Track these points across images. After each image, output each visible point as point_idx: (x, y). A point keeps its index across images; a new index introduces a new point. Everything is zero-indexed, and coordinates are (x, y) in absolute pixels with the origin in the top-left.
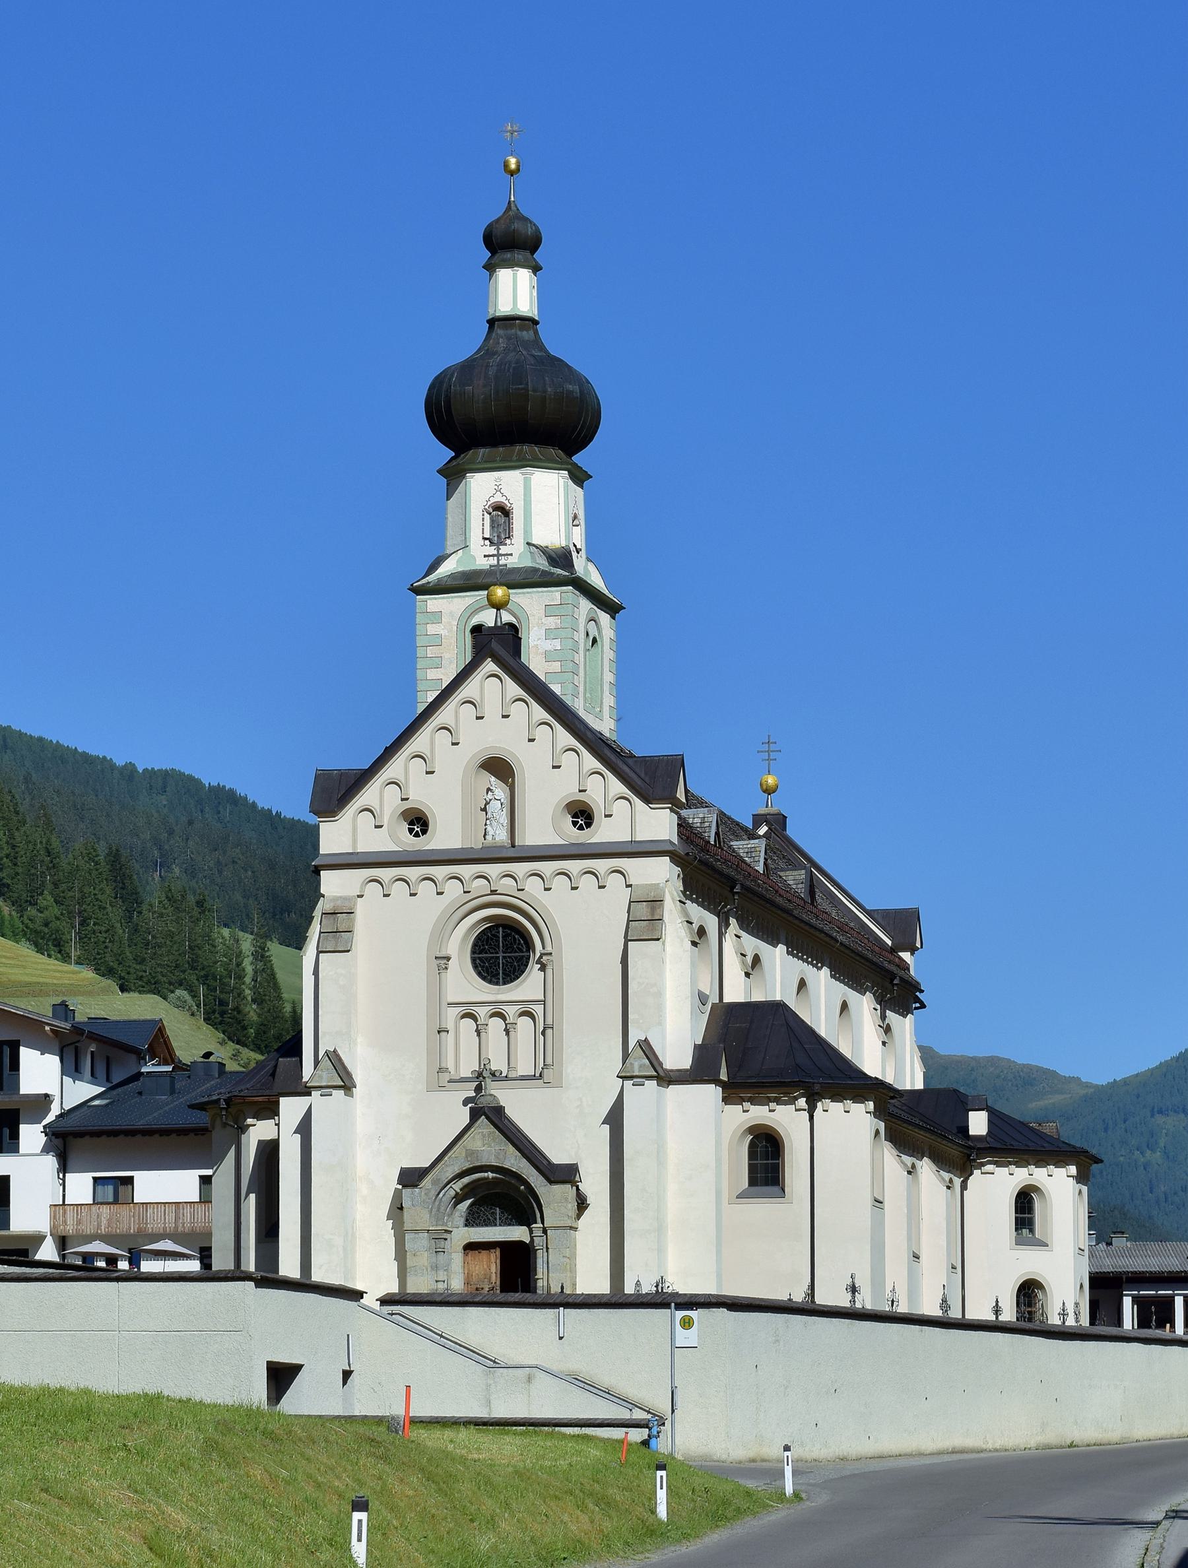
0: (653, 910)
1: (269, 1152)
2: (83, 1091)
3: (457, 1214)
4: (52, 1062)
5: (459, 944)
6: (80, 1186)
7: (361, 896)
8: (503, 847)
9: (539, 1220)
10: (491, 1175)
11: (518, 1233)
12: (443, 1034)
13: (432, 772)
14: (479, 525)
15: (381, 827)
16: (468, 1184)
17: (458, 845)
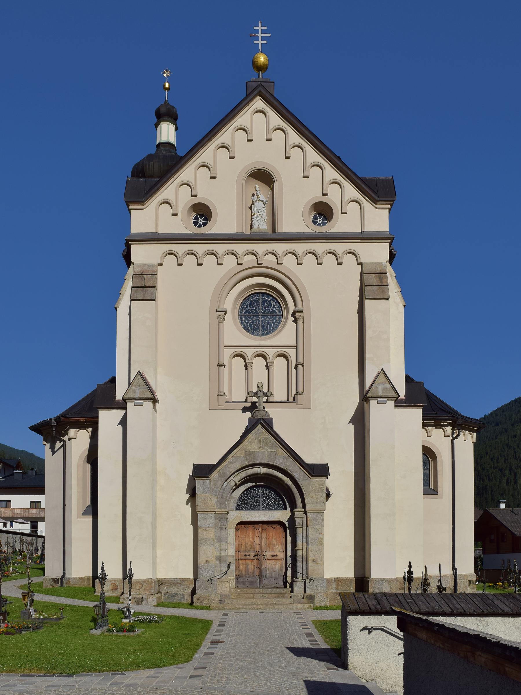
0: (381, 279)
3: (232, 500)
5: (231, 303)
7: (161, 265)
12: (221, 368)
13: (215, 178)
15: (176, 215)
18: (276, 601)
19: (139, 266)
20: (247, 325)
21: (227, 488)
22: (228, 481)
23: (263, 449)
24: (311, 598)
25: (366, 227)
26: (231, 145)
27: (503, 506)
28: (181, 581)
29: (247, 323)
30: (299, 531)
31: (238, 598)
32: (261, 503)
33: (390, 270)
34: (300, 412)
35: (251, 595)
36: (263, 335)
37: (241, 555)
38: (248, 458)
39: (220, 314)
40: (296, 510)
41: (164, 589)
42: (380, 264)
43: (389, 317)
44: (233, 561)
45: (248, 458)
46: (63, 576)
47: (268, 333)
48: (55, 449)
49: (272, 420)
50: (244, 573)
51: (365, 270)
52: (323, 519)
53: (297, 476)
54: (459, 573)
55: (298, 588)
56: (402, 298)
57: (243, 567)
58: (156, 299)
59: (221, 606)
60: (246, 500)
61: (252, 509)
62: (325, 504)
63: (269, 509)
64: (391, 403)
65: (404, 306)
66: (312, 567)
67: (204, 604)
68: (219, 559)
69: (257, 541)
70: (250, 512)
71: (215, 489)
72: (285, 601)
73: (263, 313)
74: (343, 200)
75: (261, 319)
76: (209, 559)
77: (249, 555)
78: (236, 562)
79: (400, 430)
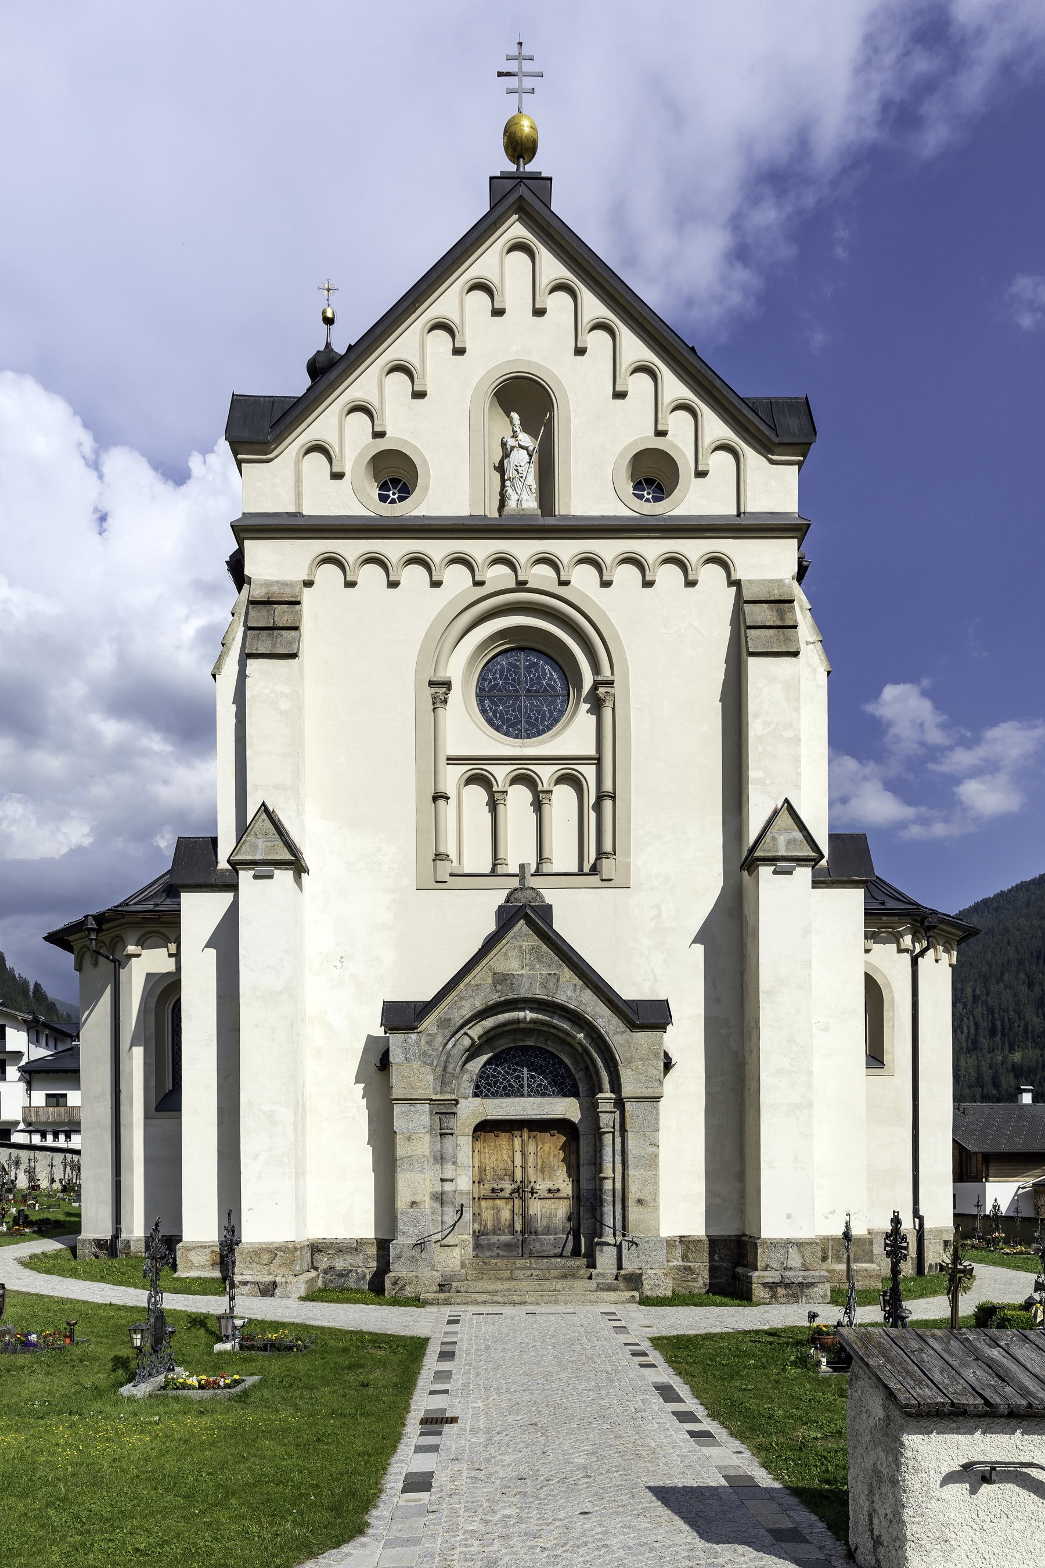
0: (781, 615)
1: (166, 993)
2: (40, 1052)
3: (466, 1077)
4: (23, 1036)
5: (460, 666)
6: (39, 1098)
7: (308, 584)
8: (532, 516)
9: (606, 1085)
10: (529, 1015)
12: (441, 803)
16: (493, 1029)
17: (465, 512)
18: (559, 1285)
19: (262, 585)
20: (495, 717)
21: (454, 1051)
22: (457, 1036)
23: (532, 968)
24: (634, 1281)
25: (749, 502)
26: (457, 321)
27: (1027, 1098)
28: (357, 1247)
29: (495, 711)
30: (607, 1139)
31: (478, 1278)
32: (526, 1083)
33: (798, 592)
34: (607, 894)
35: (507, 1273)
36: (528, 737)
37: (485, 1189)
38: (499, 987)
39: (437, 690)
40: (600, 1095)
41: (324, 1262)
42: (780, 582)
43: (792, 697)
44: (466, 1200)
45: (499, 987)
46: (116, 1236)
47: (539, 733)
49: (550, 907)
50: (490, 1225)
51: (747, 595)
52: (658, 1114)
53: (602, 1024)
54: (927, 1225)
55: (606, 1259)
56: (823, 657)
57: (488, 1215)
58: (300, 654)
59: (442, 1296)
60: (494, 1076)
61: (508, 1095)
62: (661, 1083)
63: (543, 1095)
64: (804, 874)
65: (829, 673)
66: (634, 1213)
67: (409, 1292)
68: (440, 1198)
69: (518, 1161)
70: (502, 1100)
71: (430, 1052)
72: (578, 1284)
73: (528, 691)
74: (700, 444)
75: (524, 702)
76: (418, 1199)
77: (502, 1190)
78: (474, 1203)
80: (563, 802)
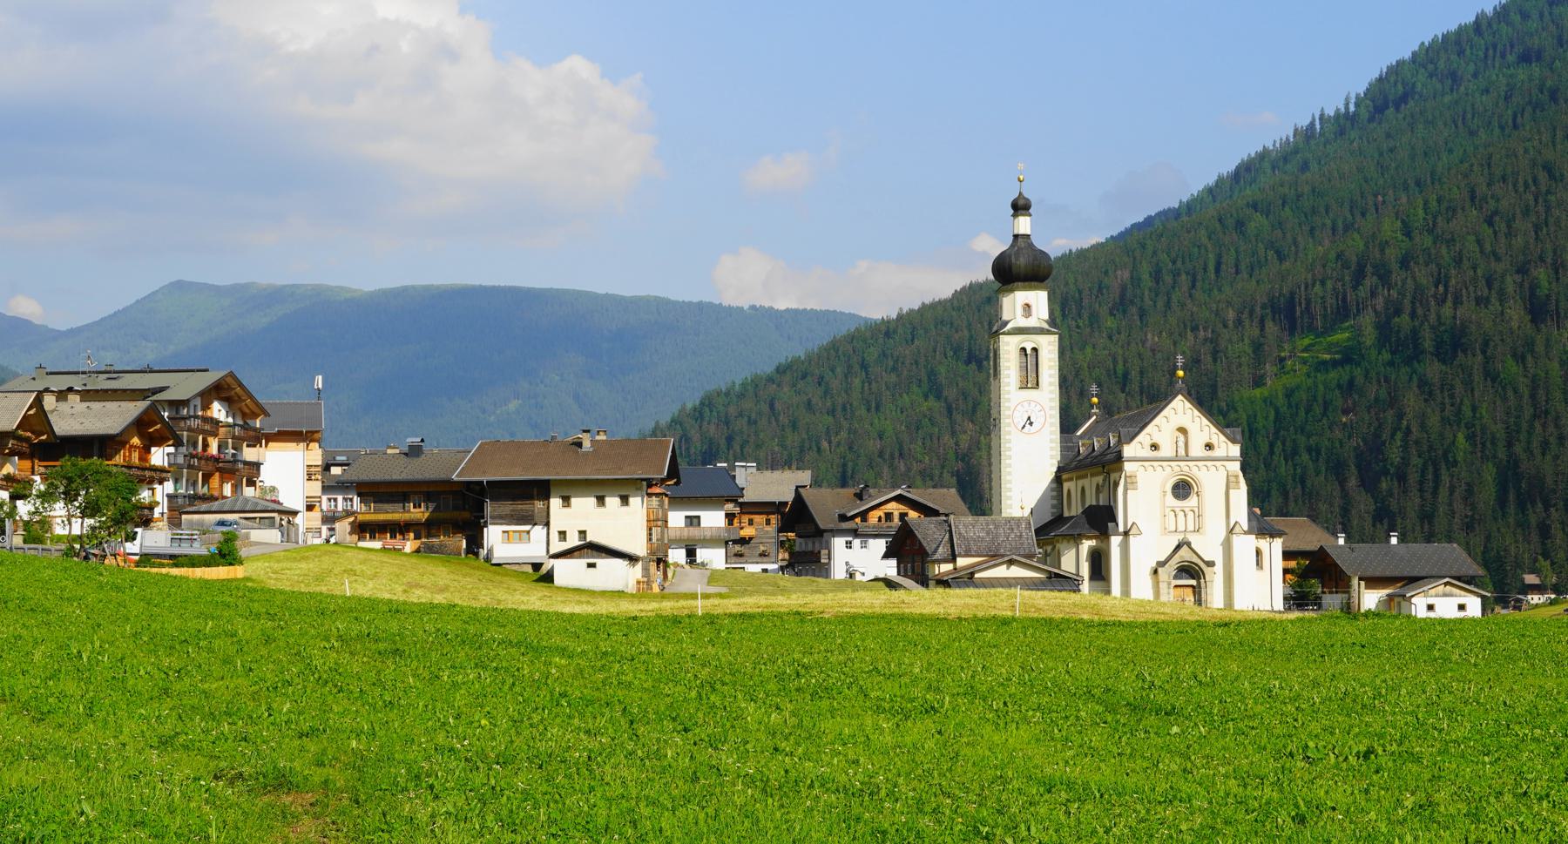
11: (1194, 582)
14: (1019, 311)
27: (1394, 541)
48: (142, 405)
79: (1246, 545)
80: (1190, 515)
